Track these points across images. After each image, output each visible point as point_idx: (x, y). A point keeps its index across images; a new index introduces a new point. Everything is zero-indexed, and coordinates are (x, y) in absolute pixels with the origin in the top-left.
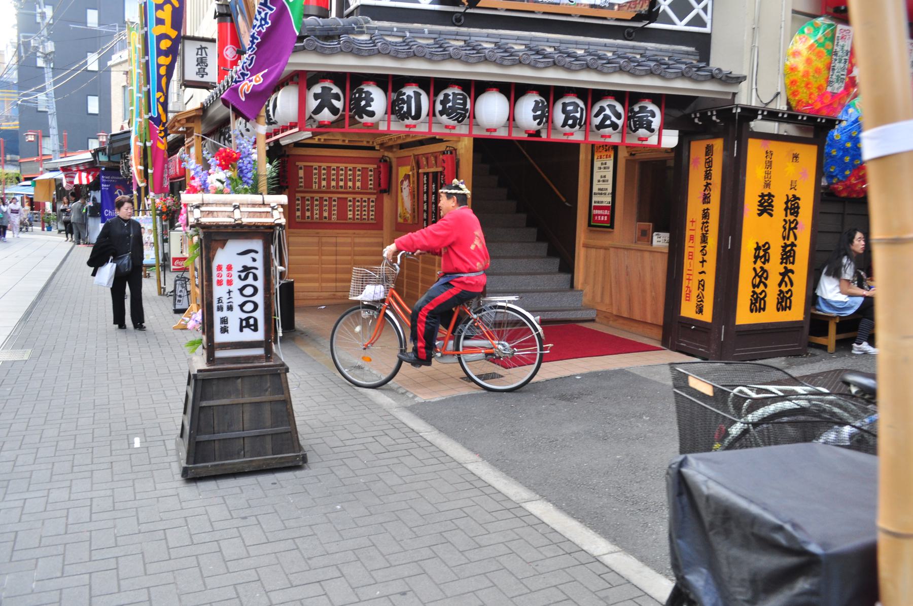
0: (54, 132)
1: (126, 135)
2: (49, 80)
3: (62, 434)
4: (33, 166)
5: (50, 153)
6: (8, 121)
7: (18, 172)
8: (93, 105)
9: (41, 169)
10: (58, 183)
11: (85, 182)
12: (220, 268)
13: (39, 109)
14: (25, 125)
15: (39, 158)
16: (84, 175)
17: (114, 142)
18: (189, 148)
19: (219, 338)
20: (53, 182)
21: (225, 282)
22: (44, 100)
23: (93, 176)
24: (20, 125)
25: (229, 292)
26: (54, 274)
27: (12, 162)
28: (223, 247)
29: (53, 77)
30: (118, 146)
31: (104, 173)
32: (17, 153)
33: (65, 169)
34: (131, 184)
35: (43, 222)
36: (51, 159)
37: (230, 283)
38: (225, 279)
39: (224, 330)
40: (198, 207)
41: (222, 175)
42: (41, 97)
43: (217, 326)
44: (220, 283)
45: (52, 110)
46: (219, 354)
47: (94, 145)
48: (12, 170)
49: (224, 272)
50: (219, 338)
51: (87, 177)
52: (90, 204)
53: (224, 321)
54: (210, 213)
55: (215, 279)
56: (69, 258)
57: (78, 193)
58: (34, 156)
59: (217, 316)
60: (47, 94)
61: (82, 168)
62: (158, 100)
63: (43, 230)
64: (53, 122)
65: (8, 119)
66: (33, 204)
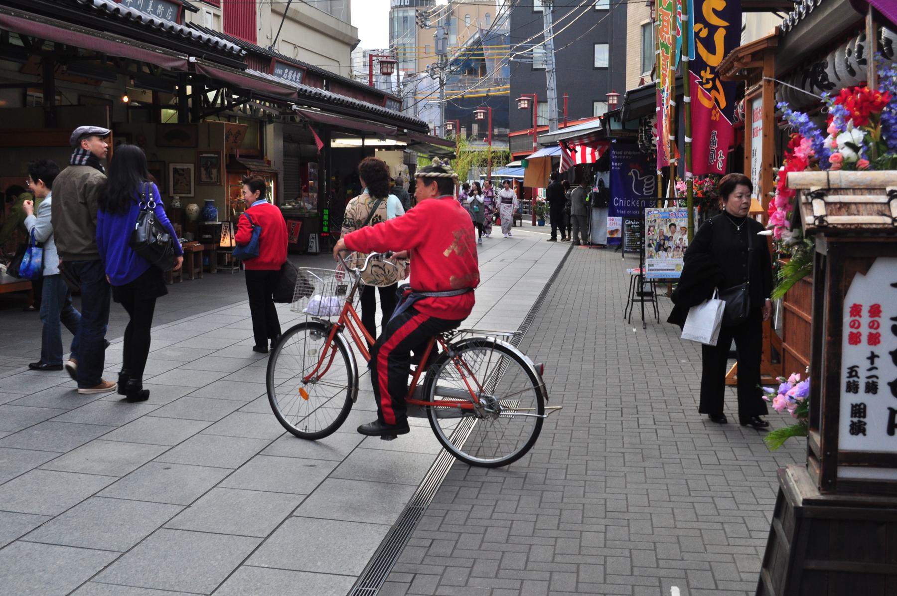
0: (551, 94)
1: (651, 91)
2: (548, 26)
3: (558, 559)
4: (526, 141)
5: (546, 122)
6: (497, 86)
7: (507, 149)
8: (602, 56)
9: (534, 145)
10: (555, 162)
11: (589, 160)
12: (856, 310)
13: (534, 67)
14: (517, 89)
15: (533, 130)
16: (589, 150)
17: (633, 101)
18: (750, 102)
19: (848, 442)
20: (549, 159)
21: (864, 338)
22: (541, 54)
23: (599, 151)
24: (511, 88)
25: (873, 357)
26: (548, 286)
27: (501, 138)
28: (865, 271)
29: (553, 23)
30: (642, 104)
31: (614, 147)
32: (507, 127)
33: (565, 144)
34: (655, 161)
35: (535, 214)
36: (547, 131)
37: (874, 339)
38: (865, 331)
39: (858, 429)
40: (820, 195)
41: (856, 135)
42: (538, 51)
43: (845, 420)
44: (855, 339)
45: (551, 66)
46: (846, 473)
47: (601, 109)
48: (500, 147)
49: (865, 319)
50: (848, 442)
51: (593, 154)
52: (596, 189)
53: (859, 410)
54: (844, 207)
55: (847, 331)
56: (566, 264)
57: (582, 174)
58: (526, 129)
59: (847, 400)
60: (545, 45)
61: (586, 141)
62: (697, 34)
63: (534, 224)
64: (551, 81)
65: (497, 83)
66: (524, 192)
